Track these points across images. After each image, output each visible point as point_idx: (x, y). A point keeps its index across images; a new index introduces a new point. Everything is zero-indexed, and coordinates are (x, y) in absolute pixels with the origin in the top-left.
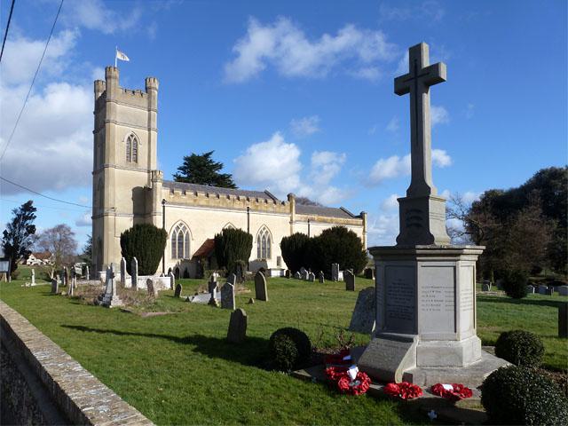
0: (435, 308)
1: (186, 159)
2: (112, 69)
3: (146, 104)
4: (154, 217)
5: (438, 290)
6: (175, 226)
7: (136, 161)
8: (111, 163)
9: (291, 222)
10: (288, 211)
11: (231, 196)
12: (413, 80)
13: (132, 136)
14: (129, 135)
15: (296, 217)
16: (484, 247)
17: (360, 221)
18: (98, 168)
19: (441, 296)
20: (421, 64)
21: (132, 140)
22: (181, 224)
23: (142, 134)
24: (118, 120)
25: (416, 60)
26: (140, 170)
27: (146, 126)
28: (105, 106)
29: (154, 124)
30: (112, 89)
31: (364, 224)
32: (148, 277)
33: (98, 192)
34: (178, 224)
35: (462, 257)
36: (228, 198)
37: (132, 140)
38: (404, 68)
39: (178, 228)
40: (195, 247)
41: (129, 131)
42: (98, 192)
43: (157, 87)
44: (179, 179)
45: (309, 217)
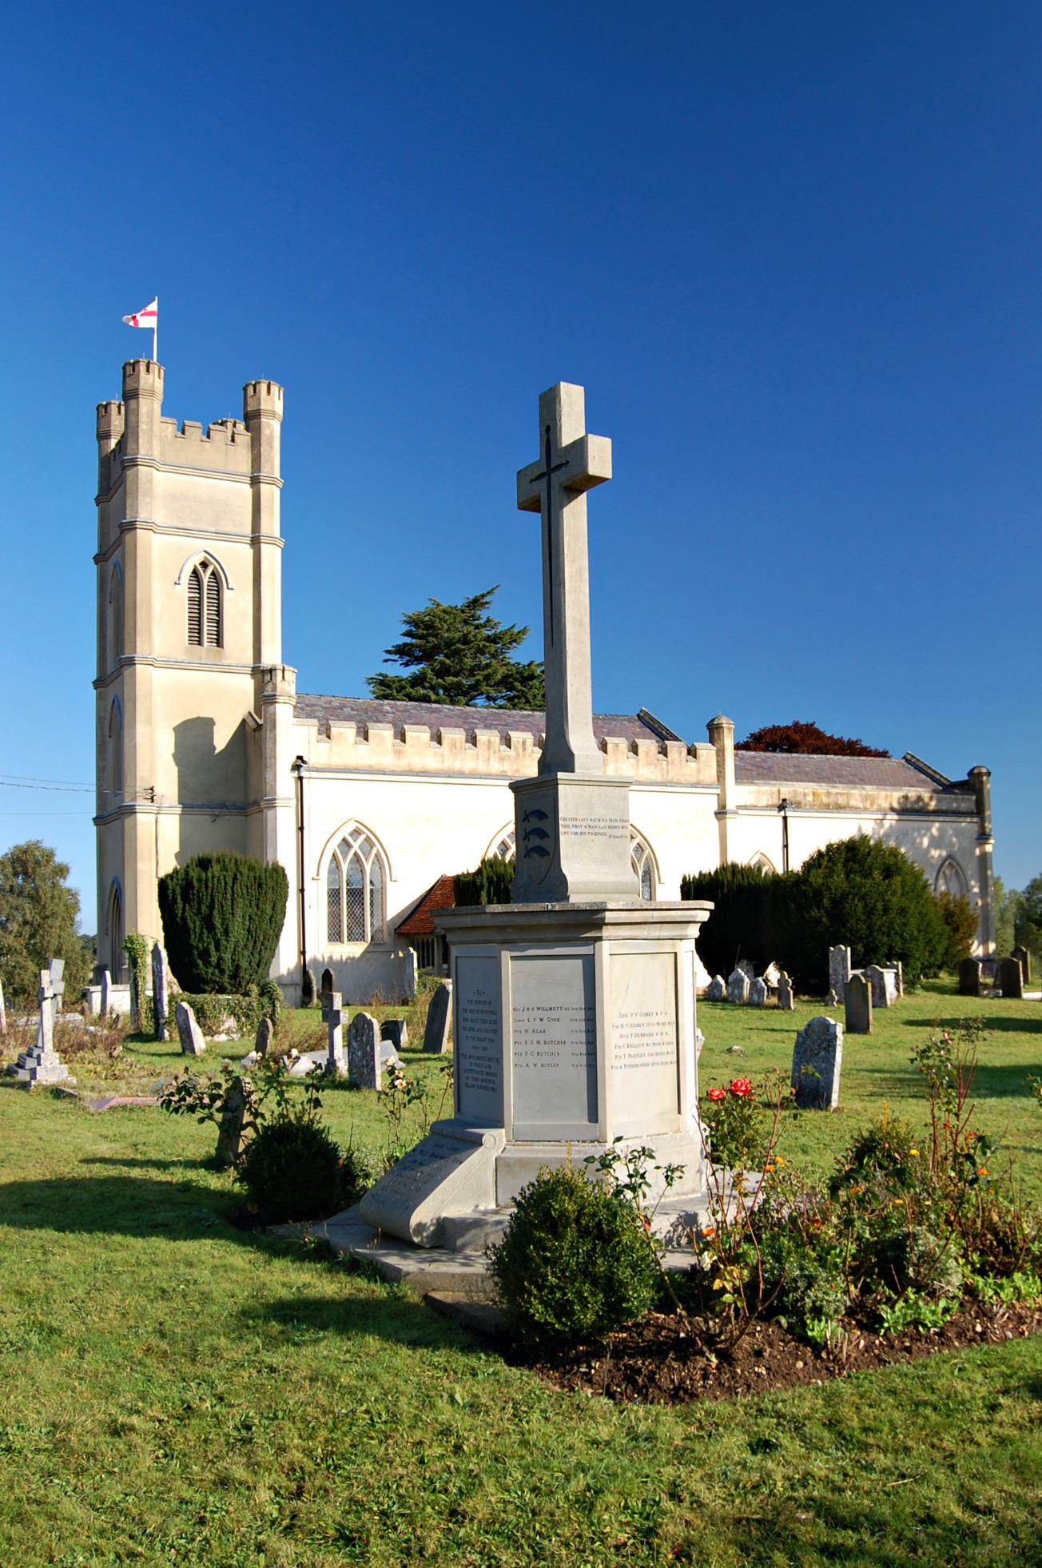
0: (546, 1059)
1: (414, 622)
2: (142, 367)
3: (245, 467)
4: (270, 813)
5: (554, 1014)
6: (337, 839)
7: (219, 642)
8: (141, 650)
9: (721, 813)
10: (711, 773)
11: (516, 736)
12: (544, 481)
13: (204, 565)
14: (196, 561)
15: (738, 794)
16: (711, 905)
17: (967, 802)
18: (110, 667)
19: (557, 1031)
20: (558, 439)
21: (206, 578)
22: (356, 833)
23: (235, 560)
24: (159, 518)
25: (548, 429)
26: (230, 669)
27: (248, 530)
28: (122, 481)
29: (271, 524)
30: (143, 427)
31: (979, 811)
32: (360, 1009)
33: (110, 743)
34: (345, 833)
35: (606, 932)
36: (507, 742)
37: (206, 578)
38: (533, 454)
39: (345, 843)
40: (400, 898)
41: (193, 551)
42: (110, 743)
43: (279, 406)
44: (386, 688)
45: (787, 789)
